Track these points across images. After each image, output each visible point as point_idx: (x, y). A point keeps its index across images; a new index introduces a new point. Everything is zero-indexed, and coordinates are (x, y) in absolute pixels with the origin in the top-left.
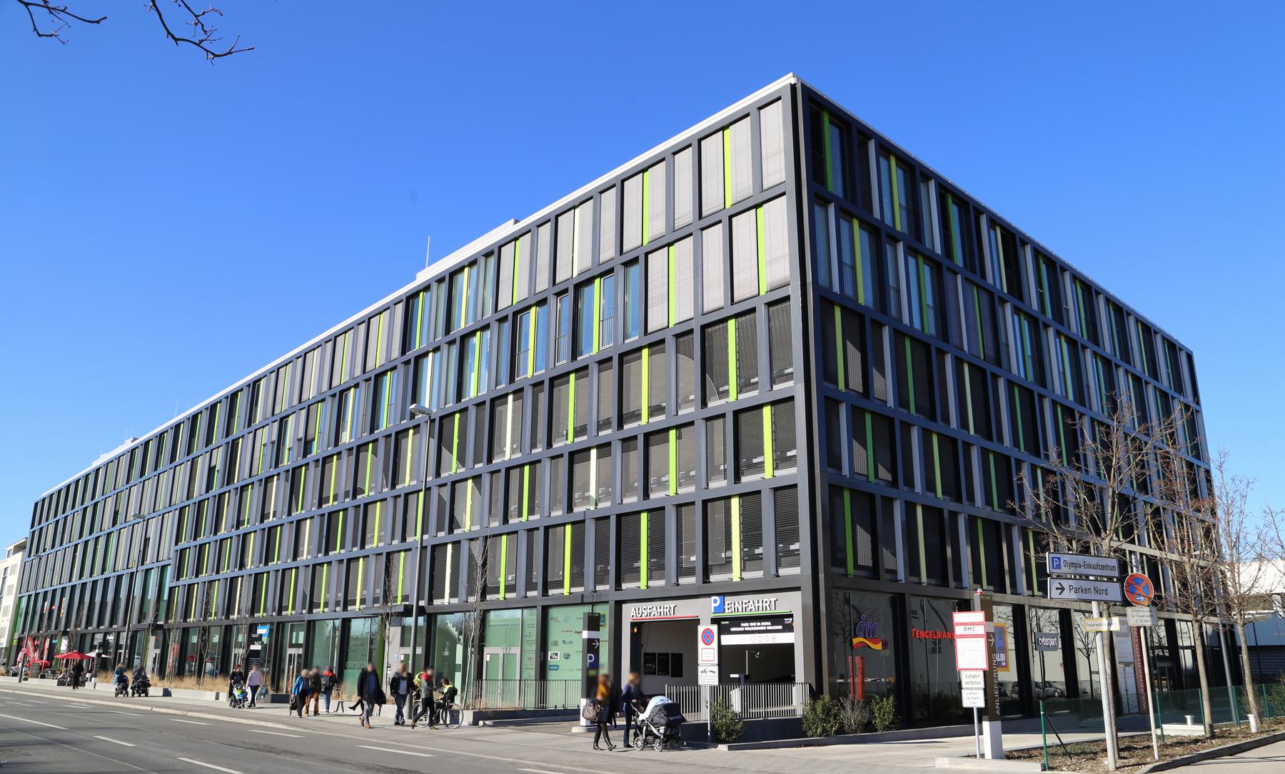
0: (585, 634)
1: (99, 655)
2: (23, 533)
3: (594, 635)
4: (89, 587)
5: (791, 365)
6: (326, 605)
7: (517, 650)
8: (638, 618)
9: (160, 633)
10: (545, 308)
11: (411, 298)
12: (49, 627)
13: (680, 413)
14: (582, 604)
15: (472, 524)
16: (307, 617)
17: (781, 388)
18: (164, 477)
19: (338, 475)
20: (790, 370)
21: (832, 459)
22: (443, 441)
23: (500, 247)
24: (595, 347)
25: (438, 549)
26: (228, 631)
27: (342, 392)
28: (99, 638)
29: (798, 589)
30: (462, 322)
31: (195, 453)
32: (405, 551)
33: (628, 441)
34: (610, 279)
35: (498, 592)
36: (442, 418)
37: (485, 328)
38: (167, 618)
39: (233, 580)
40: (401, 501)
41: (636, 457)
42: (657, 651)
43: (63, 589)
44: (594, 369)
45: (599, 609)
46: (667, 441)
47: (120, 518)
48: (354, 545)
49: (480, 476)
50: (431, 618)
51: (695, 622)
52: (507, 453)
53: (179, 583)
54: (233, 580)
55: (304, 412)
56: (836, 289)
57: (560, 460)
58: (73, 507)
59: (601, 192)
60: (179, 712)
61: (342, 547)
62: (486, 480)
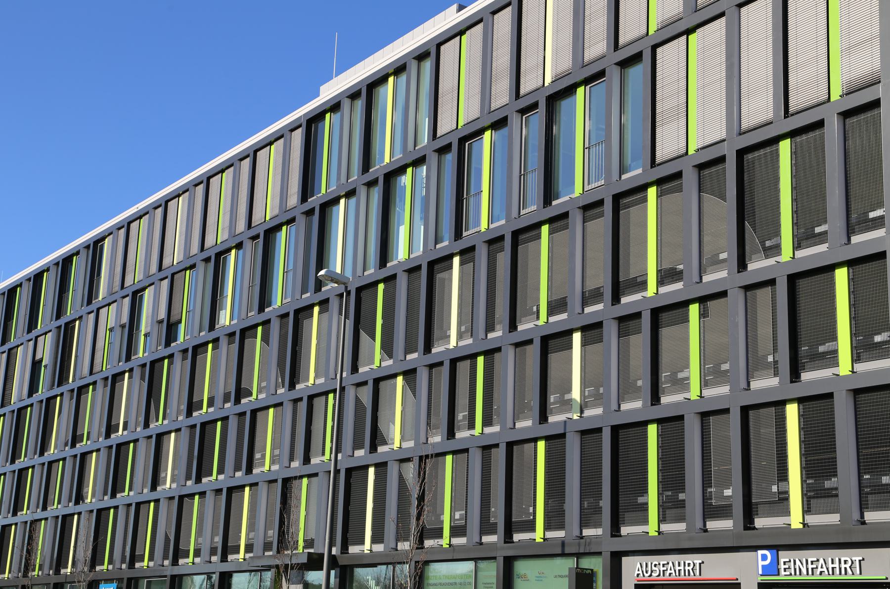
6: (197, 553)
10: (504, 131)
11: (314, 121)
13: (706, 279)
14: (563, 555)
15: (403, 439)
22: (361, 322)
23: (439, 46)
24: (577, 185)
25: (355, 474)
27: (219, 255)
30: (387, 155)
33: (628, 321)
34: (599, 87)
36: (359, 290)
37: (418, 162)
39: (67, 519)
40: (303, 406)
41: (640, 343)
44: (576, 218)
45: (587, 563)
46: (686, 320)
48: (237, 468)
52: (453, 339)
54: (67, 519)
55: (165, 284)
57: (529, 348)
61: (221, 471)
62: (423, 376)
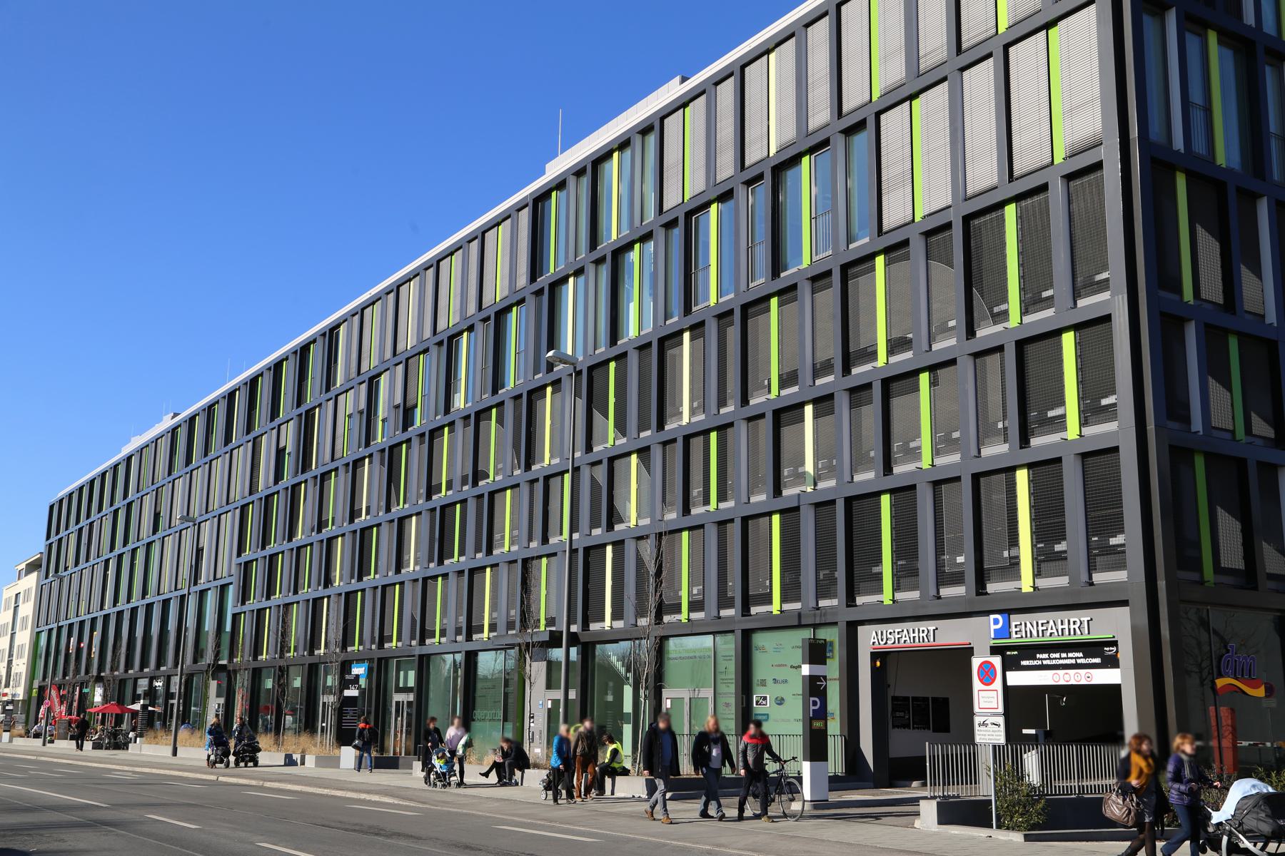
0: (806, 670)
1: (144, 707)
2: (37, 546)
3: (819, 670)
4: (127, 616)
5: (1105, 267)
7: (708, 693)
8: (881, 646)
9: (224, 675)
10: (731, 203)
11: (541, 199)
12: (77, 671)
13: (935, 347)
14: (800, 626)
15: (639, 517)
16: (418, 651)
17: (1090, 303)
18: (217, 465)
19: (451, 455)
20: (1104, 275)
21: (1175, 405)
22: (594, 402)
23: (662, 119)
24: (806, 255)
25: (592, 553)
26: (312, 672)
27: (451, 338)
28: (143, 684)
29: (1124, 603)
30: (614, 232)
31: (257, 430)
32: (548, 556)
33: (859, 392)
34: (824, 156)
35: (679, 611)
36: (591, 369)
37: (646, 237)
38: (232, 655)
39: (317, 602)
40: (539, 487)
41: (871, 414)
42: (910, 694)
43: (94, 620)
44: (805, 289)
45: (824, 634)
47: (163, 522)
48: (478, 550)
49: (647, 449)
50: (587, 650)
51: (968, 652)
52: (685, 416)
53: (245, 608)
54: (317, 602)
55: (400, 368)
56: (1178, 143)
57: (761, 422)
58: (100, 510)
59: (807, 26)
60: (254, 783)
61: (462, 553)
62: (657, 453)
